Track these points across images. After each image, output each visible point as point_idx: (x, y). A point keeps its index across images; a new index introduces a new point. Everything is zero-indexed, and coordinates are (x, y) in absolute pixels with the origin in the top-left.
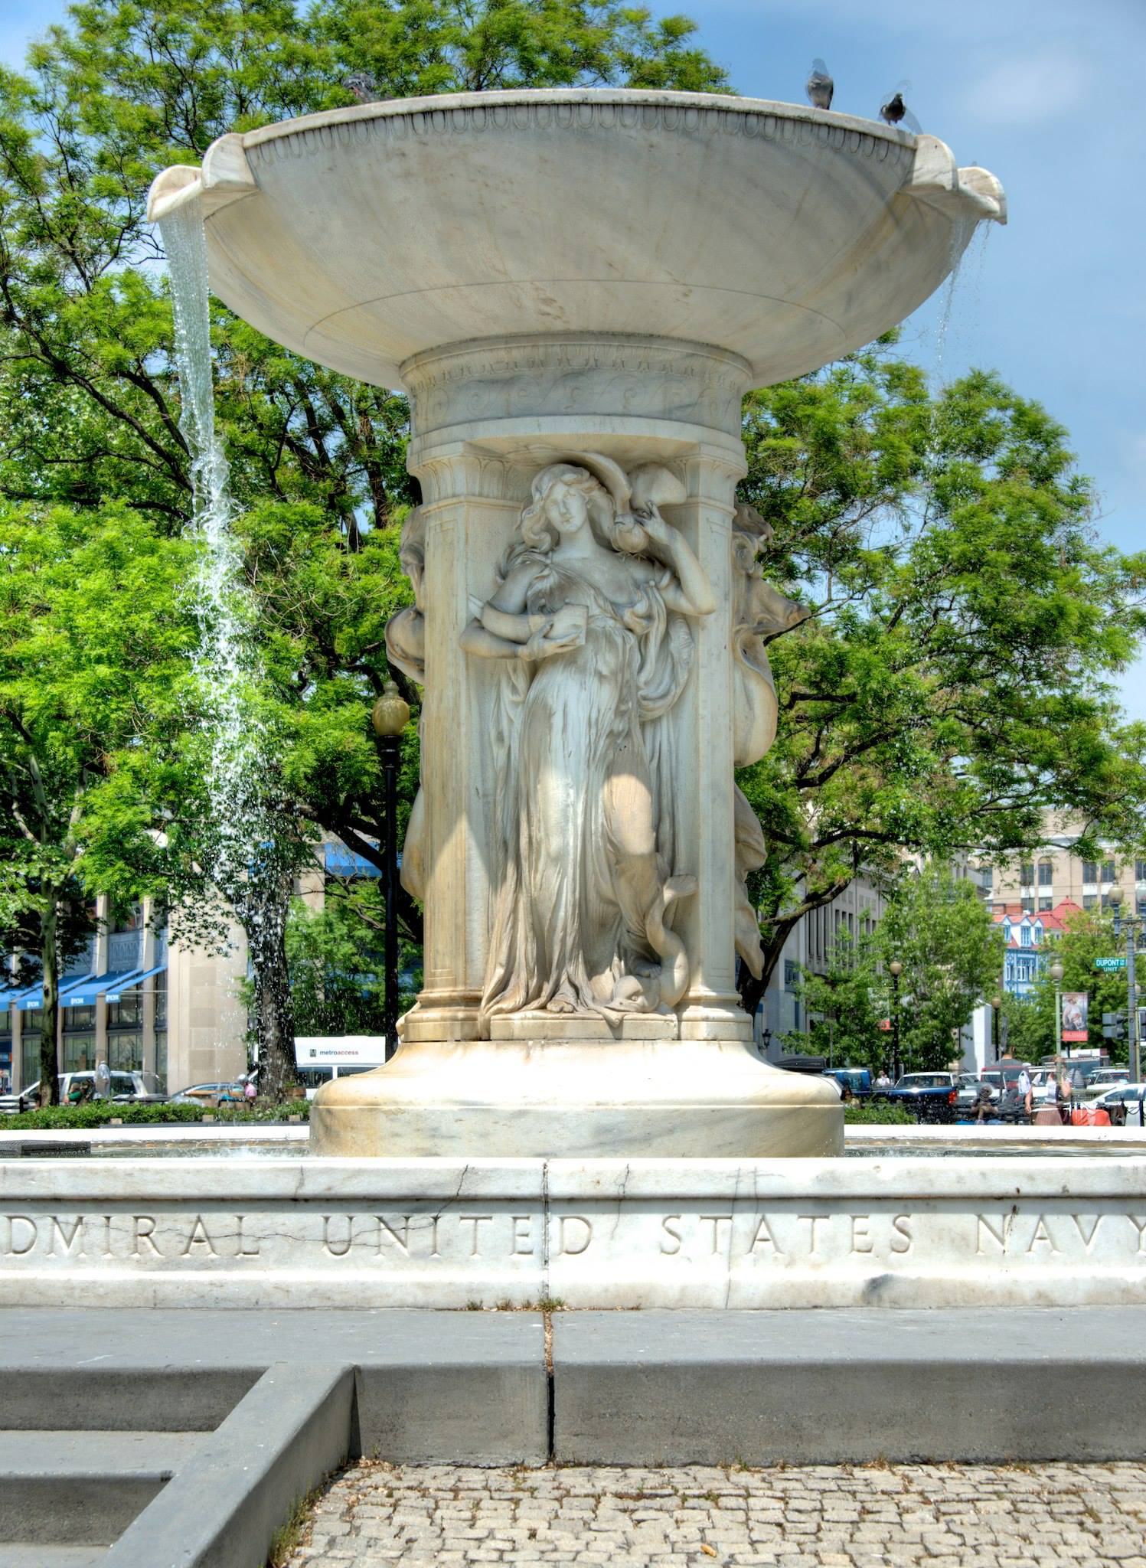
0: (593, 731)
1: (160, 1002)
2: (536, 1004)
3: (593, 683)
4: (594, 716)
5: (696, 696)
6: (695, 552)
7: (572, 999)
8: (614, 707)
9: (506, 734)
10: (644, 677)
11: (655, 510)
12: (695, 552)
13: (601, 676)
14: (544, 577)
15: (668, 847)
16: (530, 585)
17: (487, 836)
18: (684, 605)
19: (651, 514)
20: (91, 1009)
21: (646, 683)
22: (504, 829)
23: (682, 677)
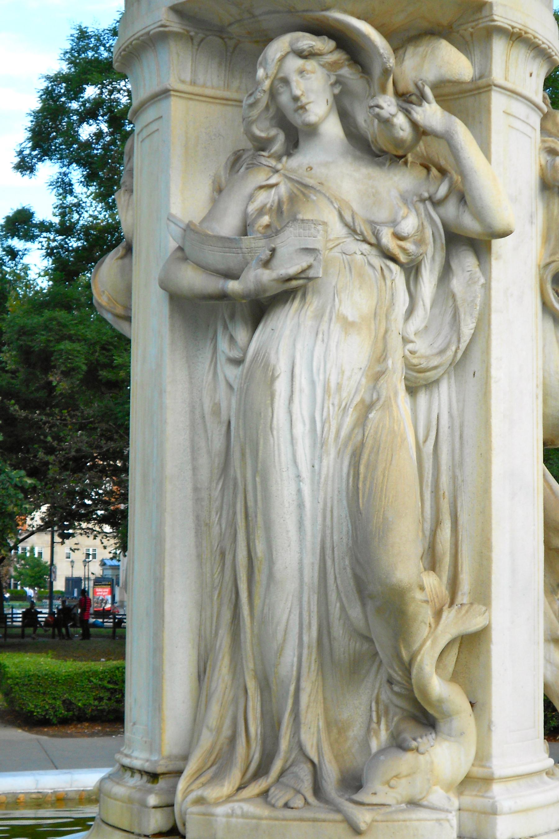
9: (224, 405)
11: (428, 91)
13: (348, 325)
14: (271, 186)
17: (199, 545)
18: (470, 224)
19: (422, 97)
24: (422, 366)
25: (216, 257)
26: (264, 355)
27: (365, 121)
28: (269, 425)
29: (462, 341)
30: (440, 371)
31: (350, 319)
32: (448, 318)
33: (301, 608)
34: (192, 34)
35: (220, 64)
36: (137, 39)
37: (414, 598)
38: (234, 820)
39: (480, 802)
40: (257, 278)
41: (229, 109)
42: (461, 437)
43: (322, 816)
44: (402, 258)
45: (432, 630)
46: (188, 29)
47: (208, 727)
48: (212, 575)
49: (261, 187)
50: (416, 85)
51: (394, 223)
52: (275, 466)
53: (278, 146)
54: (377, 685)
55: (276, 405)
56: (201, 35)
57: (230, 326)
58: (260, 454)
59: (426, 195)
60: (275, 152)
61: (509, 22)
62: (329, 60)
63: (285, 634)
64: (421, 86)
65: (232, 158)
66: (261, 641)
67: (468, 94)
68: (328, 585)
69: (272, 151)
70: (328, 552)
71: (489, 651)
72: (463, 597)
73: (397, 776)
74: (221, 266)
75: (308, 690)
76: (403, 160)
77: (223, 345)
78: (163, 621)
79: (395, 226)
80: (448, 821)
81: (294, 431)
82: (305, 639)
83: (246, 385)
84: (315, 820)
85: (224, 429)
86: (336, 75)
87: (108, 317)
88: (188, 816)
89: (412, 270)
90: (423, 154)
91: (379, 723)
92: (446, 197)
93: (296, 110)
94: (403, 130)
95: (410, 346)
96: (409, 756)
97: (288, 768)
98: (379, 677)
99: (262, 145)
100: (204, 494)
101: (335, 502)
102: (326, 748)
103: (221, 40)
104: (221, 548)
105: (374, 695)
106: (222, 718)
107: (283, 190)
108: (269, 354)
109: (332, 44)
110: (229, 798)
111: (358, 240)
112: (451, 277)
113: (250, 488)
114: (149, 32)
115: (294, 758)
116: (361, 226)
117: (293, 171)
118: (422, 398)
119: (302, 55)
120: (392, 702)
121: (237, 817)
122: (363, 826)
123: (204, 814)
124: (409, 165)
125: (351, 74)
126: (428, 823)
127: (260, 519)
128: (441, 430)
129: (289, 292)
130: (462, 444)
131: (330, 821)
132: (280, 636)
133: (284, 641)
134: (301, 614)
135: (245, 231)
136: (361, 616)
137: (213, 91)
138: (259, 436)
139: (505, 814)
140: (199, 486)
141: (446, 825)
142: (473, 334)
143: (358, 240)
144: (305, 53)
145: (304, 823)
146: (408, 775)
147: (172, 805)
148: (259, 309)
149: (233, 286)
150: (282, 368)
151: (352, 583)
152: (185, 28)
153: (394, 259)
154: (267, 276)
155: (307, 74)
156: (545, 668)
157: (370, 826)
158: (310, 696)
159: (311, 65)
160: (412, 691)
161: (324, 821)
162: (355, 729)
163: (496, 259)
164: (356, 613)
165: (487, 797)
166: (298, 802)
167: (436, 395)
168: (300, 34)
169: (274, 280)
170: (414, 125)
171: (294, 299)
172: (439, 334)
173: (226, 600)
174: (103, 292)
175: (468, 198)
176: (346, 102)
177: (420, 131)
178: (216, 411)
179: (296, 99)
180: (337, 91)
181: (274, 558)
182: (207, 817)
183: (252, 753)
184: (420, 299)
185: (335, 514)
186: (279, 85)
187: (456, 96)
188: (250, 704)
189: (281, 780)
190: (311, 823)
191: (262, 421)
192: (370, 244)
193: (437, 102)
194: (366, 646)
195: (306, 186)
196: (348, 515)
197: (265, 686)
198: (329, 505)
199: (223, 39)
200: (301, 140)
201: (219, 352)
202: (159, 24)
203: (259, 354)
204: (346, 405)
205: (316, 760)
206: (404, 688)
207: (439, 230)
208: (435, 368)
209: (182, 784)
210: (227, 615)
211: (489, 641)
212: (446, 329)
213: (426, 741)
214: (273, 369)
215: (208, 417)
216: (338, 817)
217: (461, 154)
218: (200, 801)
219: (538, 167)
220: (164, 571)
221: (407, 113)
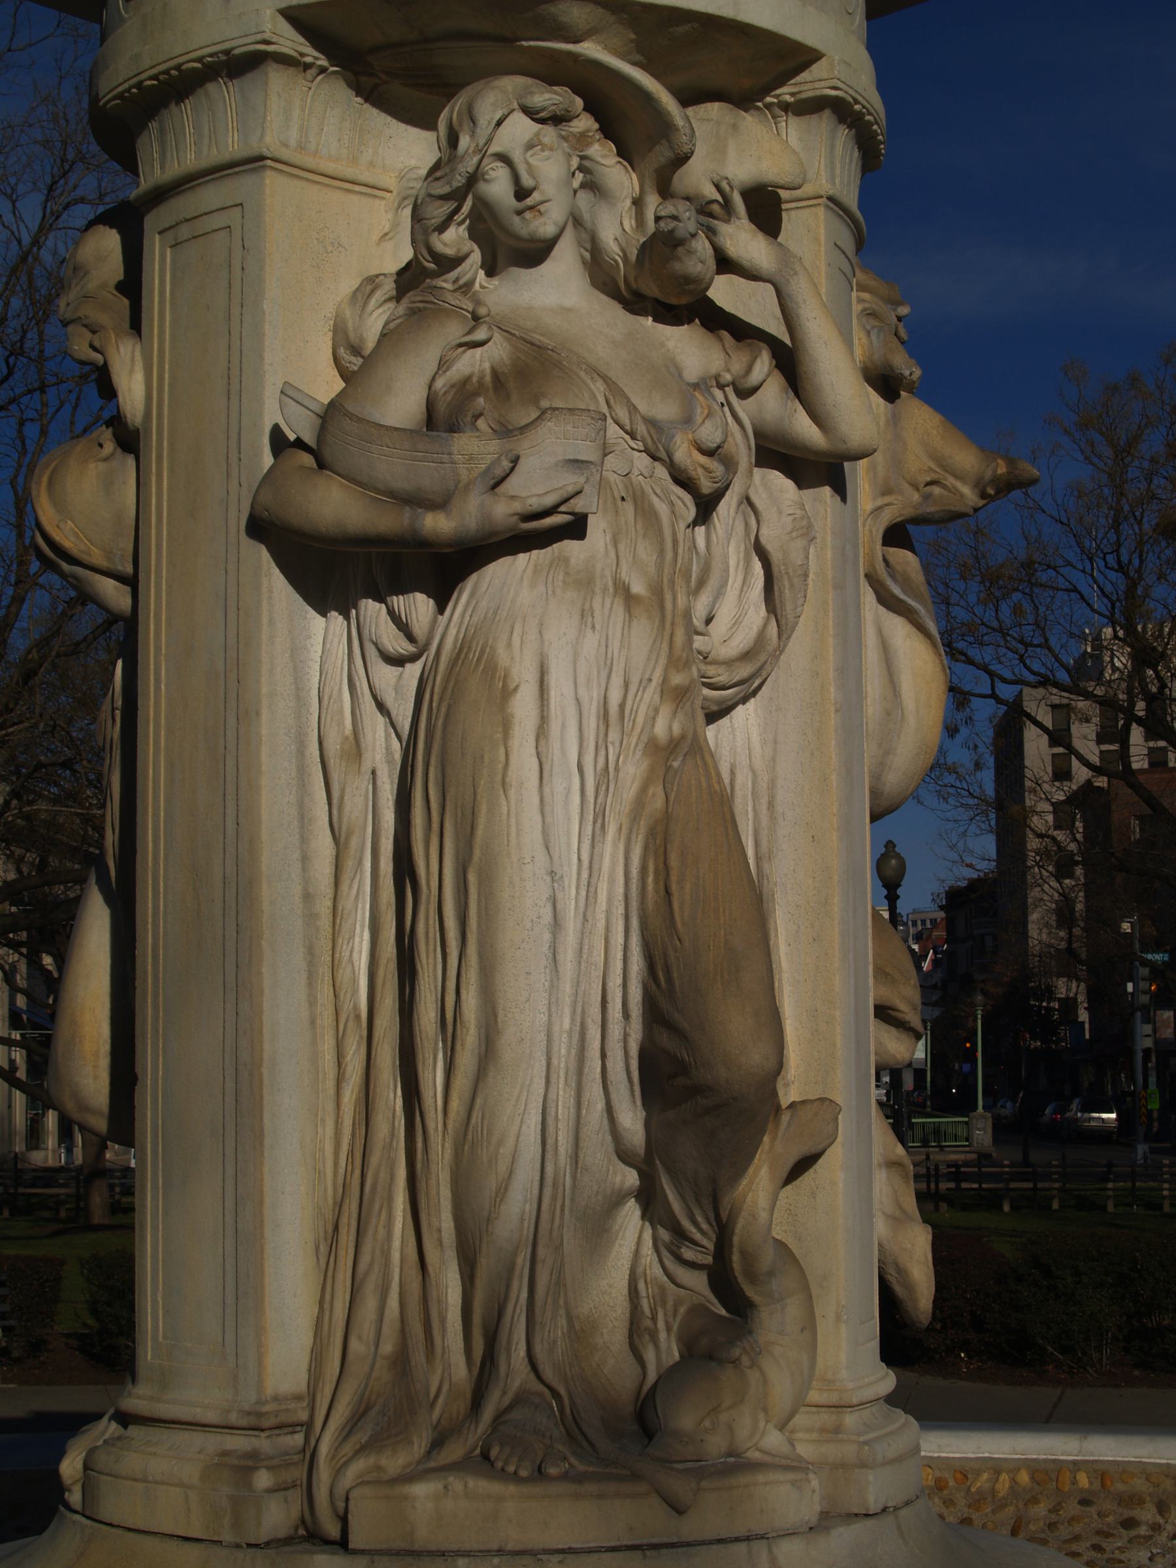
2: (454, 1451)
16: (443, 364)
18: (804, 428)
25: (393, 467)
28: (499, 778)
36: (199, 60)
47: (360, 1338)
49: (460, 345)
55: (515, 743)
58: (480, 832)
59: (728, 377)
64: (727, 188)
74: (401, 484)
78: (262, 1144)
81: (547, 790)
91: (654, 1319)
108: (493, 649)
114: (233, 49)
116: (641, 429)
119: (530, 113)
130: (773, 818)
132: (503, 1167)
138: (479, 797)
159: (549, 134)
162: (605, 1331)
181: (500, 1023)
202: (259, 37)
203: (470, 648)
205: (562, 1391)
214: (505, 676)
220: (262, 1051)
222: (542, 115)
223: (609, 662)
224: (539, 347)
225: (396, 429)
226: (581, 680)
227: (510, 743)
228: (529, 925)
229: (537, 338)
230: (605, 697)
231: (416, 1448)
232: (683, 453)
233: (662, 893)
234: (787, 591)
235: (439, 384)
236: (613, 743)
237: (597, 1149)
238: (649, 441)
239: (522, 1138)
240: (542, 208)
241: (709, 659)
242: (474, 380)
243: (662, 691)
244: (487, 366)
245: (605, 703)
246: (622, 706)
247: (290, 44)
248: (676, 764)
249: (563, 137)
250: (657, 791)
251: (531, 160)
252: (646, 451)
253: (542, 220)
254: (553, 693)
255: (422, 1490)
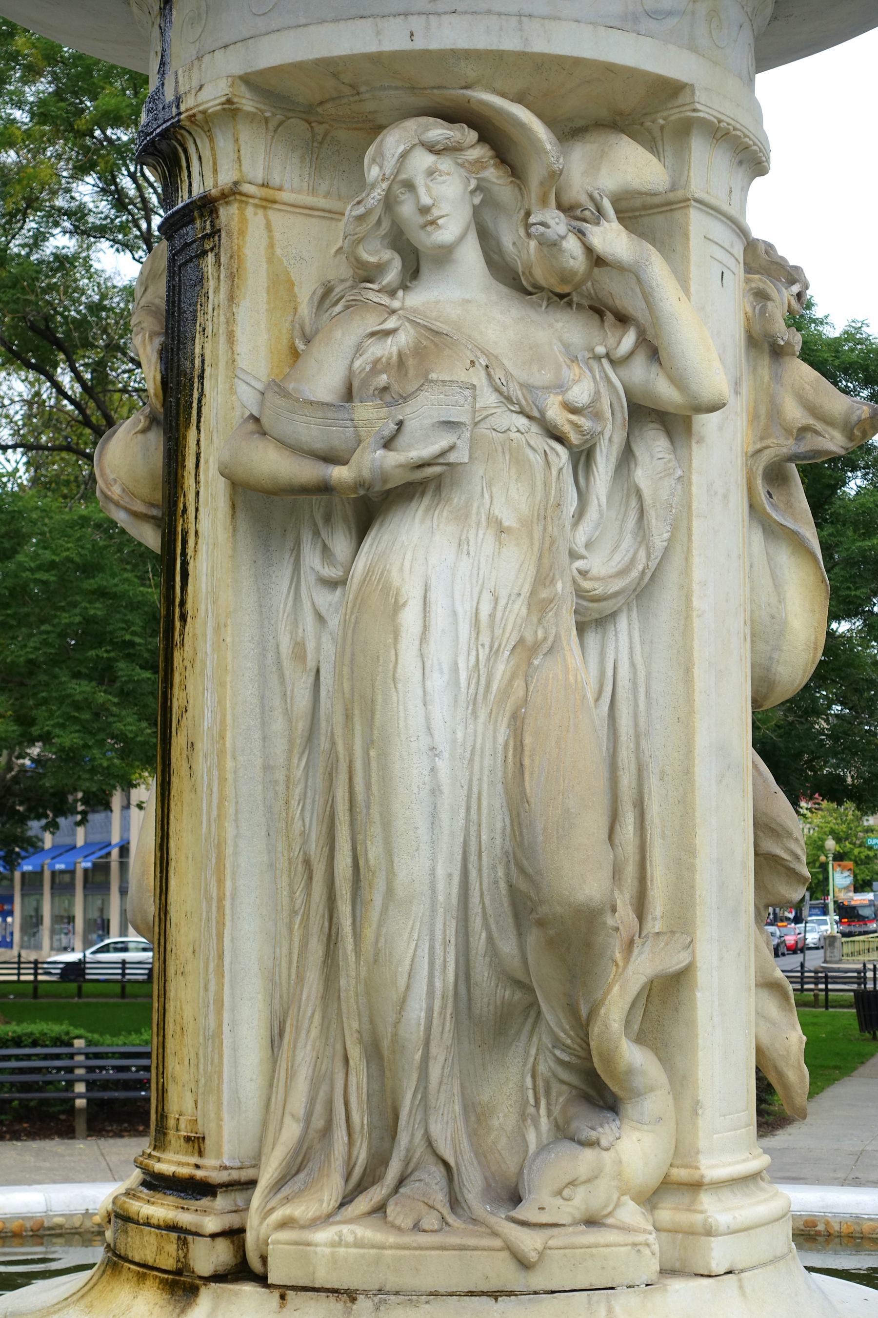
0: (485, 638)
1: (123, 866)
2: (363, 1203)
3: (483, 541)
4: (485, 610)
5: (686, 572)
6: (683, 281)
7: (440, 1198)
8: (526, 589)
9: (310, 646)
10: (581, 536)
11: (607, 205)
12: (683, 281)
14: (388, 333)
15: (630, 871)
16: (359, 349)
18: (665, 391)
20: (72, 872)
21: (588, 545)
22: (304, 835)
23: (659, 537)
24: (597, 592)
25: (310, 431)
26: (382, 574)
27: (514, 244)
29: (653, 557)
30: (621, 600)
31: (506, 523)
32: (631, 523)
33: (432, 939)
34: (268, 114)
35: (302, 158)
37: (605, 923)
38: (342, 1250)
39: (684, 1218)
40: (372, 462)
41: (314, 221)
42: (647, 693)
43: (472, 1242)
44: (574, 438)
45: (620, 970)
46: (262, 107)
48: (292, 893)
49: (373, 334)
50: (591, 197)
51: (560, 387)
52: (399, 735)
53: (392, 276)
54: (533, 1051)
55: (403, 645)
56: (279, 117)
57: (324, 535)
58: (378, 716)
59: (601, 350)
60: (388, 284)
61: (715, 113)
62: (470, 158)
63: (409, 979)
64: (598, 197)
65: (320, 292)
66: (370, 989)
67: (656, 210)
68: (471, 906)
69: (384, 283)
70: (473, 858)
71: (693, 1000)
72: (655, 925)
73: (572, 1183)
74: (319, 445)
75: (441, 1059)
76: (566, 300)
77: (311, 559)
79: (564, 393)
80: (648, 1245)
81: (428, 683)
82: (438, 984)
83: (354, 616)
84: (462, 1248)
85: (311, 679)
86: (478, 179)
87: (121, 517)
88: (270, 1247)
89: (583, 458)
90: (590, 294)
91: (537, 1105)
92: (631, 354)
93: (424, 227)
94: (573, 258)
95: (579, 564)
96: (588, 1154)
97: (411, 1173)
98: (535, 1039)
99: (367, 275)
100: (280, 776)
101: (485, 786)
102: (465, 1144)
103: (307, 125)
104: (305, 853)
105: (529, 1066)
106: (312, 1101)
107: (404, 339)
108: (389, 572)
109: (473, 135)
110: (327, 1219)
111: (512, 411)
112: (633, 466)
113: (358, 765)
115: (421, 1157)
116: (516, 392)
117: (415, 311)
118: (592, 639)
119: (432, 148)
120: (555, 1075)
121: (347, 1245)
122: (533, 1256)
123: (297, 1243)
124: (574, 306)
125: (498, 178)
126: (622, 1249)
127: (375, 811)
128: (620, 684)
129: (423, 485)
131: (484, 1249)
133: (408, 987)
134: (432, 948)
135: (349, 395)
136: (515, 951)
137: (294, 195)
139: (721, 1235)
140: (271, 763)
141: (646, 1251)
142: (666, 548)
143: (512, 411)
144: (439, 147)
145: (447, 1253)
146: (588, 1181)
147: (242, 1231)
148: (370, 509)
149: (339, 473)
150: (412, 594)
151: (506, 902)
152: (259, 106)
153: (560, 439)
154: (392, 459)
155: (440, 175)
156: (757, 1025)
157: (541, 1254)
158: (443, 1068)
159: (445, 164)
160: (589, 1058)
161: (475, 1249)
162: (501, 1115)
163: (698, 442)
164: (508, 947)
165: (695, 1211)
166: (431, 1221)
167: (611, 634)
168: (431, 119)
169: (401, 466)
170: (589, 250)
171: (423, 494)
172: (617, 547)
173: (315, 930)
174: (115, 480)
175: (662, 354)
176: (488, 218)
177: (597, 260)
178: (299, 652)
179: (424, 210)
180: (477, 200)
182: (301, 1247)
183: (355, 1153)
184: (594, 497)
185: (485, 803)
186: (398, 190)
187: (637, 214)
188: (353, 1080)
189: (402, 1190)
190: (770, 1268)
191: (380, 669)
192: (529, 417)
193: (620, 220)
194: (518, 995)
195: (437, 333)
196: (505, 804)
197: (375, 1053)
198: (475, 790)
199: (310, 123)
200: (424, 269)
201: (305, 569)
204: (500, 645)
205: (452, 1163)
206: (575, 1056)
207: (620, 399)
208: (615, 595)
209: (257, 1197)
210: (316, 949)
211: (693, 987)
212: (628, 540)
213: (606, 1133)
215: (286, 663)
216: (498, 1243)
217: (656, 294)
218: (285, 1224)
219: (742, 317)
221: (581, 234)
222: (437, 148)
223: (480, 582)
224: (437, 332)
225: (327, 404)
226: (457, 596)
227: (399, 646)
228: (416, 790)
229: (438, 326)
230: (477, 609)
231: (325, 1205)
232: (555, 413)
233: (518, 765)
234: (654, 521)
235: (357, 364)
236: (483, 645)
237: (482, 972)
238: (523, 402)
239: (417, 960)
240: (440, 222)
241: (589, 575)
242: (384, 360)
243: (529, 604)
244: (395, 350)
245: (477, 613)
246: (492, 616)
247: (251, 103)
248: (536, 662)
249: (462, 166)
250: (519, 683)
251: (431, 184)
252: (522, 412)
253: (440, 232)
254: (433, 607)
255: (323, 1235)
